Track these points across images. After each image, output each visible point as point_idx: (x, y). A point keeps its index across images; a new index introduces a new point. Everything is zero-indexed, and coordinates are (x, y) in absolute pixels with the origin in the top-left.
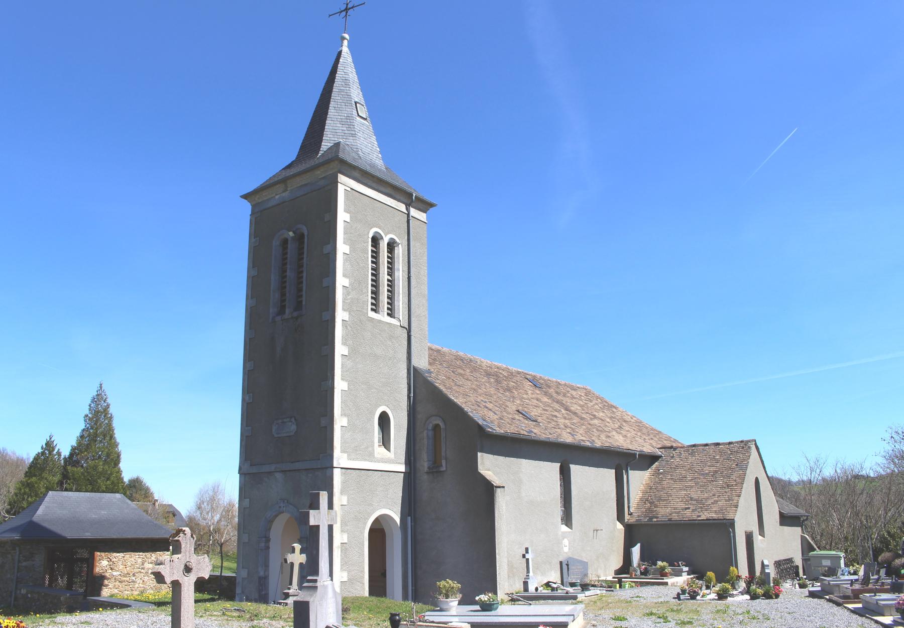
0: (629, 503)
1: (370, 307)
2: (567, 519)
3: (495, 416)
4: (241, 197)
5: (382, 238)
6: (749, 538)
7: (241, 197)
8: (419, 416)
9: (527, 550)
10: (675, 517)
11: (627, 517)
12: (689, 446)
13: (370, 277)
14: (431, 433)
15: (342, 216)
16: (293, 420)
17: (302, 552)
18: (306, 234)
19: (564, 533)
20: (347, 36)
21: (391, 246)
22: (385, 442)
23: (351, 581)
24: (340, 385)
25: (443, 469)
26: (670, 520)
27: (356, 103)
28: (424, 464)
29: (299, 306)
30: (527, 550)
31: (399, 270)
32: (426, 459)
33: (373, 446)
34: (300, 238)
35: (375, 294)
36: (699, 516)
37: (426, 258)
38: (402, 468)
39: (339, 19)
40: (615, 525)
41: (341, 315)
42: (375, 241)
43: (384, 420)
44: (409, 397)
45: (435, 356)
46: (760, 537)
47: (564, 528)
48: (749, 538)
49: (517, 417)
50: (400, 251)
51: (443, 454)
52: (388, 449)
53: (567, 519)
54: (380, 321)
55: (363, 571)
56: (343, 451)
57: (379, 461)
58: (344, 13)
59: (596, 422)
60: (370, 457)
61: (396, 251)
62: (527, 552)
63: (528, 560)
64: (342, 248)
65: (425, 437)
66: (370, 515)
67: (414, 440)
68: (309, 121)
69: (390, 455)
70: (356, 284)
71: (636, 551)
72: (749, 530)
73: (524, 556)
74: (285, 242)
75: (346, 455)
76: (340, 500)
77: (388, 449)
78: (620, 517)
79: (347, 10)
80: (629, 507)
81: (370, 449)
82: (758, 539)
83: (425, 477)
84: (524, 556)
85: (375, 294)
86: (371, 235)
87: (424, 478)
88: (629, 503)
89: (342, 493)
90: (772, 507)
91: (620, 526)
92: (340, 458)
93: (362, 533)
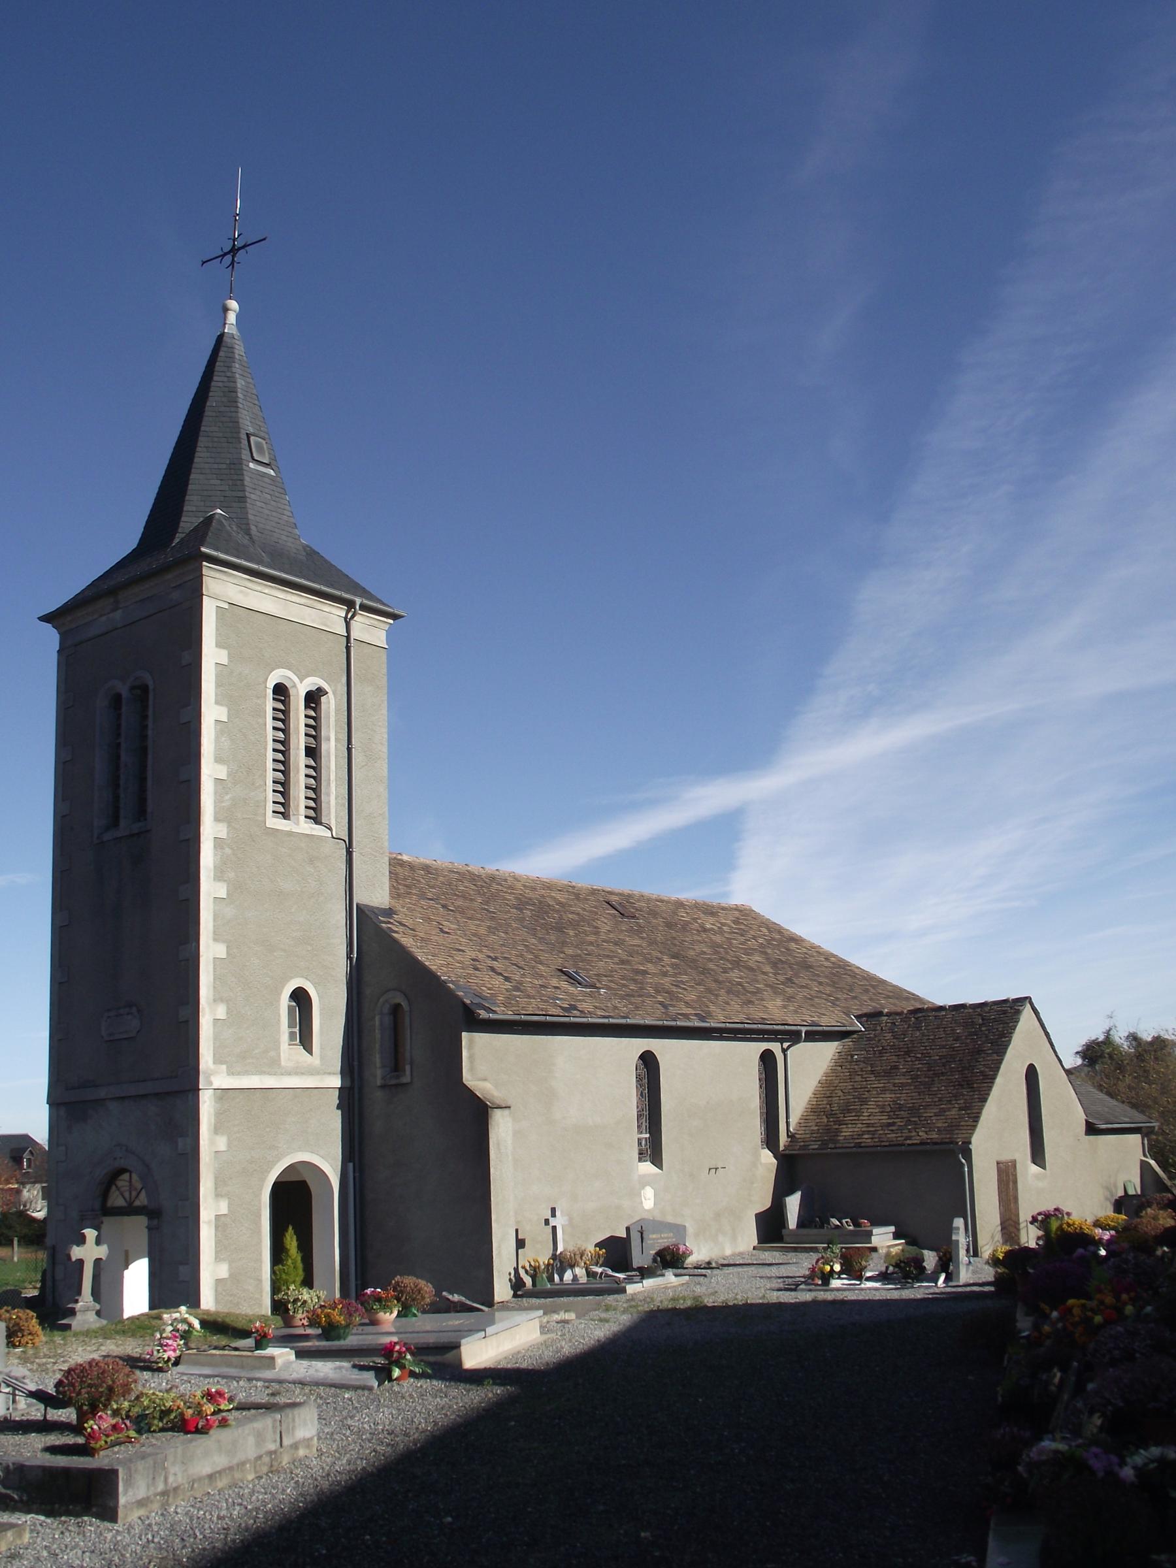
0: (787, 1117)
1: (270, 807)
2: (653, 1151)
3: (490, 988)
4: (42, 619)
5: (295, 686)
6: (1007, 1175)
7: (42, 619)
8: (368, 991)
9: (553, 1211)
10: (866, 1139)
11: (783, 1139)
12: (911, 1012)
13: (270, 755)
14: (388, 1020)
15: (212, 656)
16: (134, 1010)
17: (98, 1242)
18: (151, 688)
19: (642, 1177)
20: (233, 304)
21: (313, 698)
22: (305, 1039)
23: (235, 1277)
24: (210, 950)
25: (406, 1079)
26: (858, 1145)
27: (248, 436)
28: (377, 1072)
29: (141, 812)
30: (553, 1211)
31: (328, 739)
32: (378, 1065)
33: (277, 1048)
34: (142, 693)
35: (284, 787)
36: (909, 1138)
37: (385, 712)
38: (337, 1082)
39: (219, 269)
40: (757, 1156)
41: (210, 830)
42: (281, 691)
43: (300, 998)
44: (349, 957)
45: (404, 875)
46: (1034, 1169)
47: (647, 1167)
48: (1007, 1175)
49: (554, 982)
50: (331, 705)
51: (408, 1055)
52: (310, 1052)
53: (653, 1151)
54: (290, 834)
55: (259, 1260)
56: (218, 1060)
57: (289, 1073)
58: (228, 258)
59: (735, 975)
60: (273, 1066)
61: (323, 706)
62: (554, 1215)
63: (554, 1228)
64: (212, 713)
65: (378, 1023)
66: (271, 1165)
67: (360, 1031)
68: (183, 417)
69: (314, 1060)
70: (243, 773)
71: (793, 1203)
72: (1006, 1157)
73: (547, 1222)
74: (117, 700)
75: (224, 1067)
76: (212, 1142)
77: (310, 1052)
78: (770, 1140)
79: (234, 251)
80: (788, 1123)
81: (272, 1054)
82: (1029, 1171)
83: (379, 1094)
84: (547, 1222)
85: (284, 787)
86: (271, 685)
87: (376, 1098)
88: (787, 1117)
89: (217, 1130)
90: (1064, 1108)
91: (768, 1159)
92: (215, 1075)
93: (258, 1195)
